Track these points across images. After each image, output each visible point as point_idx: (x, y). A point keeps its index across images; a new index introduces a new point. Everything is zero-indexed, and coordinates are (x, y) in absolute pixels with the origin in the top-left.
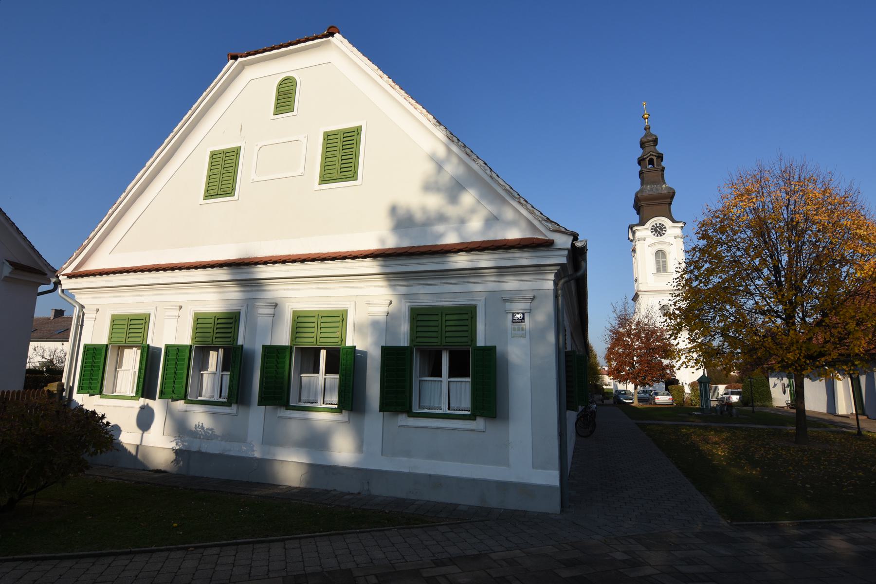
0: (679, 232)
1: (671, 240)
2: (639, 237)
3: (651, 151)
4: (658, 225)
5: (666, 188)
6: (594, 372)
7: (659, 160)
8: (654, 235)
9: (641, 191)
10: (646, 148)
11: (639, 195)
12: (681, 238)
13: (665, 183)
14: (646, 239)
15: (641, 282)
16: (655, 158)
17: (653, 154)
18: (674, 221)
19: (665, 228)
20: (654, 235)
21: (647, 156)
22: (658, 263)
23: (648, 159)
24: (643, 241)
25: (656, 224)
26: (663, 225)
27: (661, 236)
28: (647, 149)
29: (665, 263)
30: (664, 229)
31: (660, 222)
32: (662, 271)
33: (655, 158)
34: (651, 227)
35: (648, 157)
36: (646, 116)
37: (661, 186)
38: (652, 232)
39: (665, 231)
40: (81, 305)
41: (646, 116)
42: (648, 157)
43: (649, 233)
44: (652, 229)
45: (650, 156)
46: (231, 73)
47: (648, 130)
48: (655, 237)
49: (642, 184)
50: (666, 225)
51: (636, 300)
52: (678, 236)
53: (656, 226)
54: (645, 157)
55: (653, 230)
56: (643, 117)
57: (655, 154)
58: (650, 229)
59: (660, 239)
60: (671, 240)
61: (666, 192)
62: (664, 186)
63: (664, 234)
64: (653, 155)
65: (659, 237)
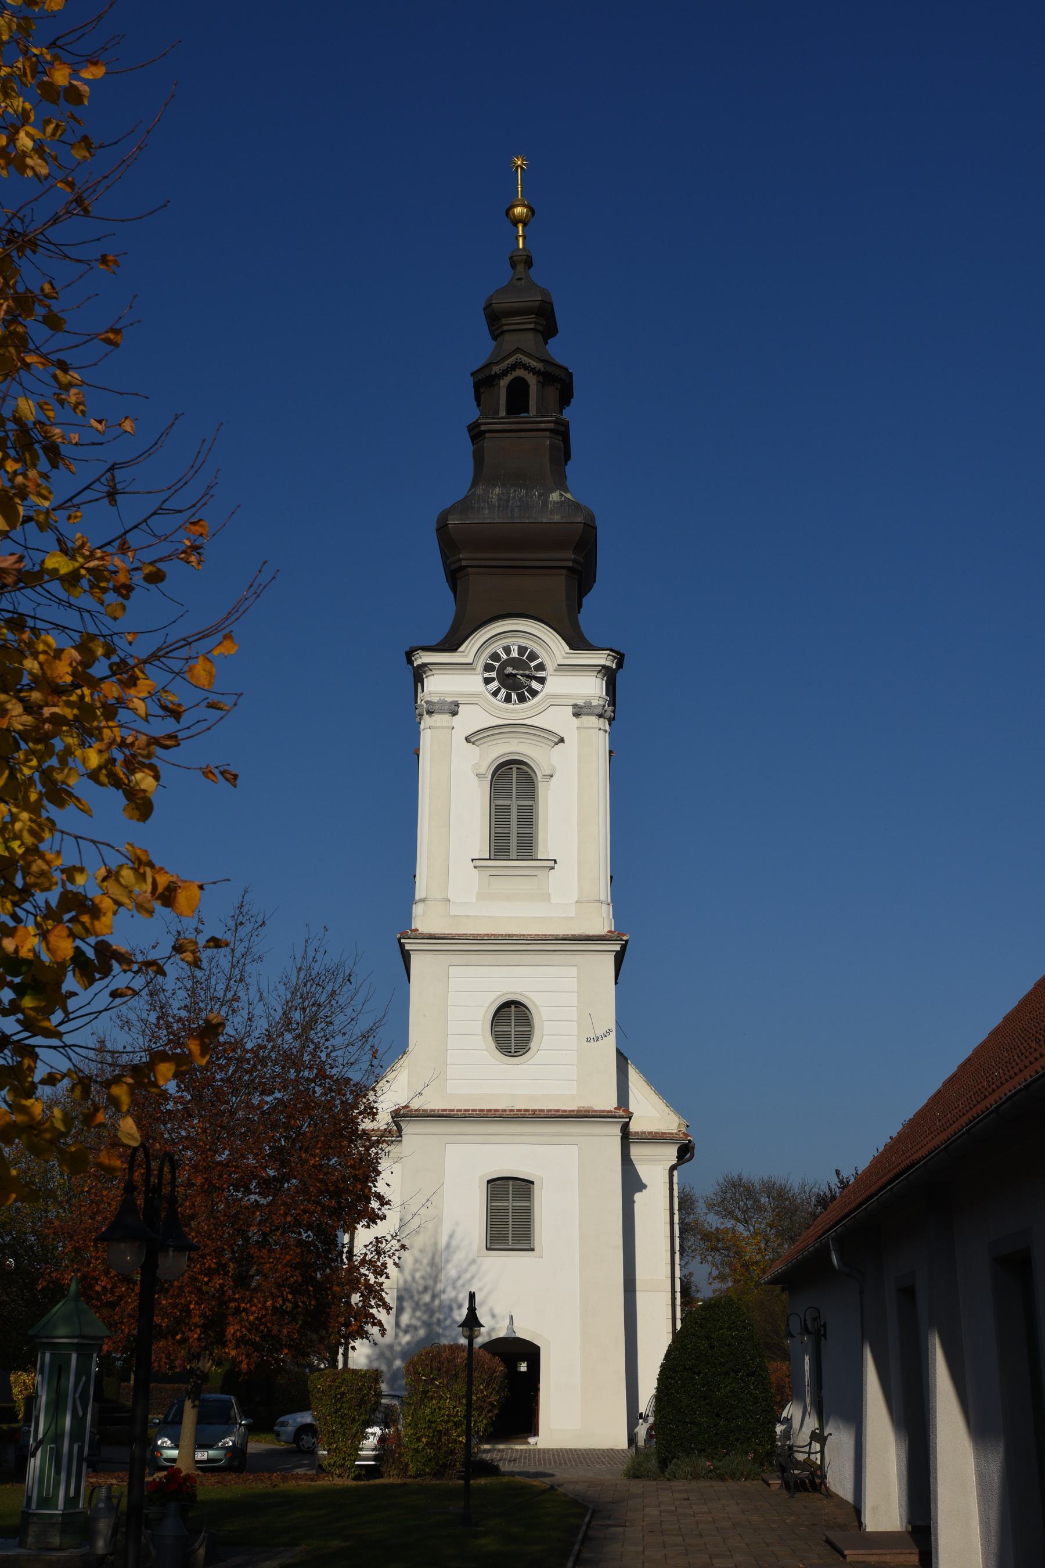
0: (593, 688)
1: (560, 720)
2: (435, 699)
3: (518, 350)
4: (515, 654)
5: (562, 503)
6: (241, 1404)
7: (552, 393)
8: (495, 694)
9: (464, 506)
10: (507, 336)
11: (452, 521)
12: (600, 716)
13: (561, 483)
14: (461, 709)
15: (423, 896)
16: (532, 380)
17: (525, 360)
18: (577, 641)
19: (541, 667)
20: (495, 694)
21: (504, 365)
22: (498, 816)
23: (504, 382)
24: (447, 717)
25: (507, 649)
26: (533, 656)
27: (522, 699)
28: (510, 341)
29: (528, 818)
30: (493, 675)
31: (524, 642)
32: (513, 854)
33: (532, 380)
34: (484, 658)
35: (505, 373)
36: (518, 210)
37: (544, 496)
38: (487, 681)
39: (542, 681)
40: (454, 589)
41: (518, 210)
42: (505, 373)
43: (472, 683)
44: (488, 668)
45: (514, 367)
46: (82, 1391)
47: (520, 268)
48: (497, 702)
49: (475, 483)
50: (544, 657)
51: (174, 902)
52: (588, 705)
53: (504, 656)
54: (496, 369)
55: (493, 675)
56: (507, 213)
57: (534, 364)
58: (480, 666)
59: (516, 712)
60: (560, 720)
61: (557, 518)
62: (555, 496)
63: (534, 693)
64: (526, 367)
65: (515, 706)
